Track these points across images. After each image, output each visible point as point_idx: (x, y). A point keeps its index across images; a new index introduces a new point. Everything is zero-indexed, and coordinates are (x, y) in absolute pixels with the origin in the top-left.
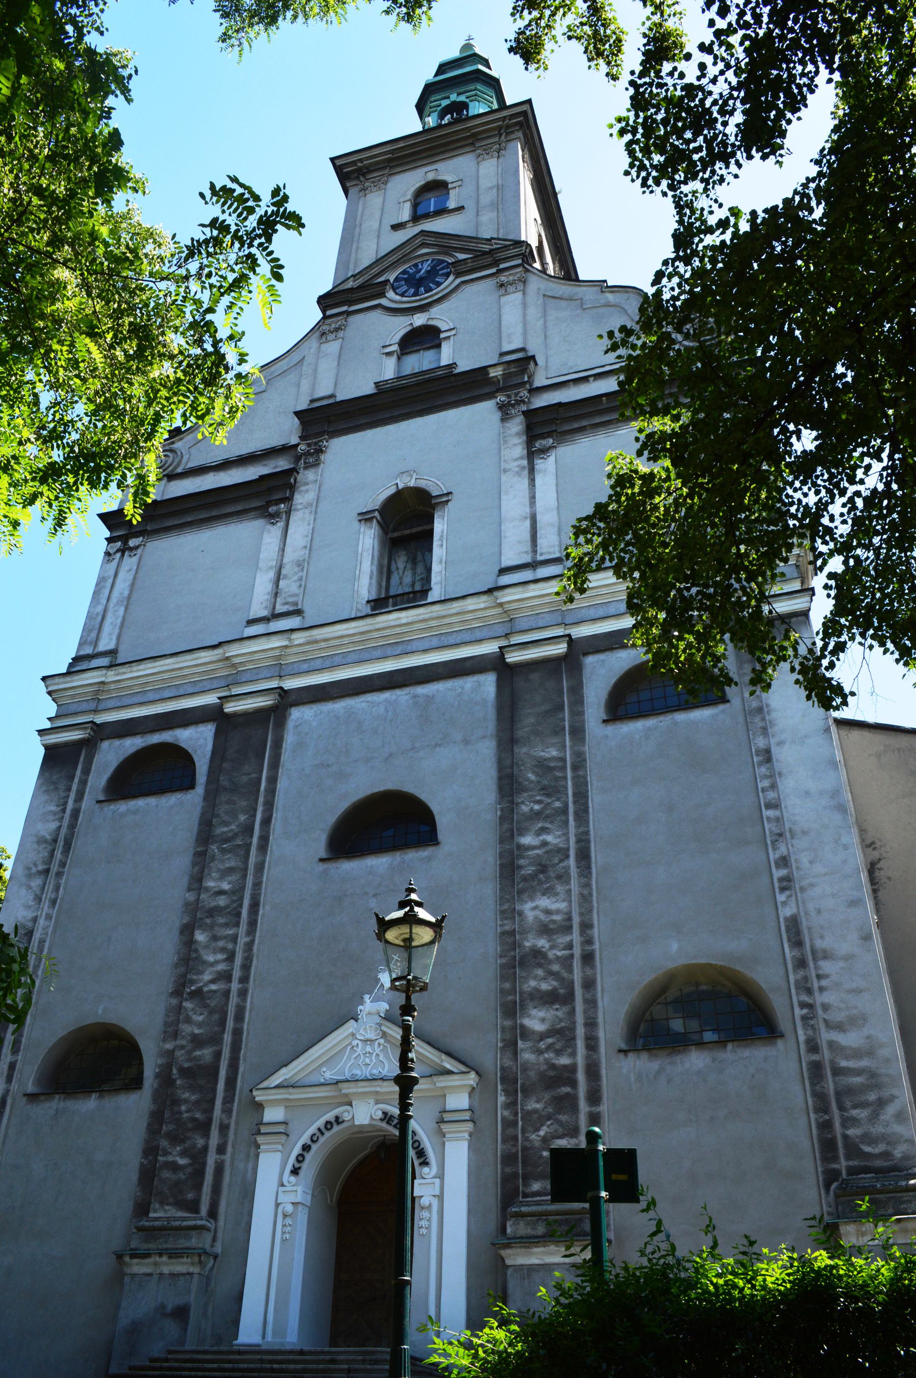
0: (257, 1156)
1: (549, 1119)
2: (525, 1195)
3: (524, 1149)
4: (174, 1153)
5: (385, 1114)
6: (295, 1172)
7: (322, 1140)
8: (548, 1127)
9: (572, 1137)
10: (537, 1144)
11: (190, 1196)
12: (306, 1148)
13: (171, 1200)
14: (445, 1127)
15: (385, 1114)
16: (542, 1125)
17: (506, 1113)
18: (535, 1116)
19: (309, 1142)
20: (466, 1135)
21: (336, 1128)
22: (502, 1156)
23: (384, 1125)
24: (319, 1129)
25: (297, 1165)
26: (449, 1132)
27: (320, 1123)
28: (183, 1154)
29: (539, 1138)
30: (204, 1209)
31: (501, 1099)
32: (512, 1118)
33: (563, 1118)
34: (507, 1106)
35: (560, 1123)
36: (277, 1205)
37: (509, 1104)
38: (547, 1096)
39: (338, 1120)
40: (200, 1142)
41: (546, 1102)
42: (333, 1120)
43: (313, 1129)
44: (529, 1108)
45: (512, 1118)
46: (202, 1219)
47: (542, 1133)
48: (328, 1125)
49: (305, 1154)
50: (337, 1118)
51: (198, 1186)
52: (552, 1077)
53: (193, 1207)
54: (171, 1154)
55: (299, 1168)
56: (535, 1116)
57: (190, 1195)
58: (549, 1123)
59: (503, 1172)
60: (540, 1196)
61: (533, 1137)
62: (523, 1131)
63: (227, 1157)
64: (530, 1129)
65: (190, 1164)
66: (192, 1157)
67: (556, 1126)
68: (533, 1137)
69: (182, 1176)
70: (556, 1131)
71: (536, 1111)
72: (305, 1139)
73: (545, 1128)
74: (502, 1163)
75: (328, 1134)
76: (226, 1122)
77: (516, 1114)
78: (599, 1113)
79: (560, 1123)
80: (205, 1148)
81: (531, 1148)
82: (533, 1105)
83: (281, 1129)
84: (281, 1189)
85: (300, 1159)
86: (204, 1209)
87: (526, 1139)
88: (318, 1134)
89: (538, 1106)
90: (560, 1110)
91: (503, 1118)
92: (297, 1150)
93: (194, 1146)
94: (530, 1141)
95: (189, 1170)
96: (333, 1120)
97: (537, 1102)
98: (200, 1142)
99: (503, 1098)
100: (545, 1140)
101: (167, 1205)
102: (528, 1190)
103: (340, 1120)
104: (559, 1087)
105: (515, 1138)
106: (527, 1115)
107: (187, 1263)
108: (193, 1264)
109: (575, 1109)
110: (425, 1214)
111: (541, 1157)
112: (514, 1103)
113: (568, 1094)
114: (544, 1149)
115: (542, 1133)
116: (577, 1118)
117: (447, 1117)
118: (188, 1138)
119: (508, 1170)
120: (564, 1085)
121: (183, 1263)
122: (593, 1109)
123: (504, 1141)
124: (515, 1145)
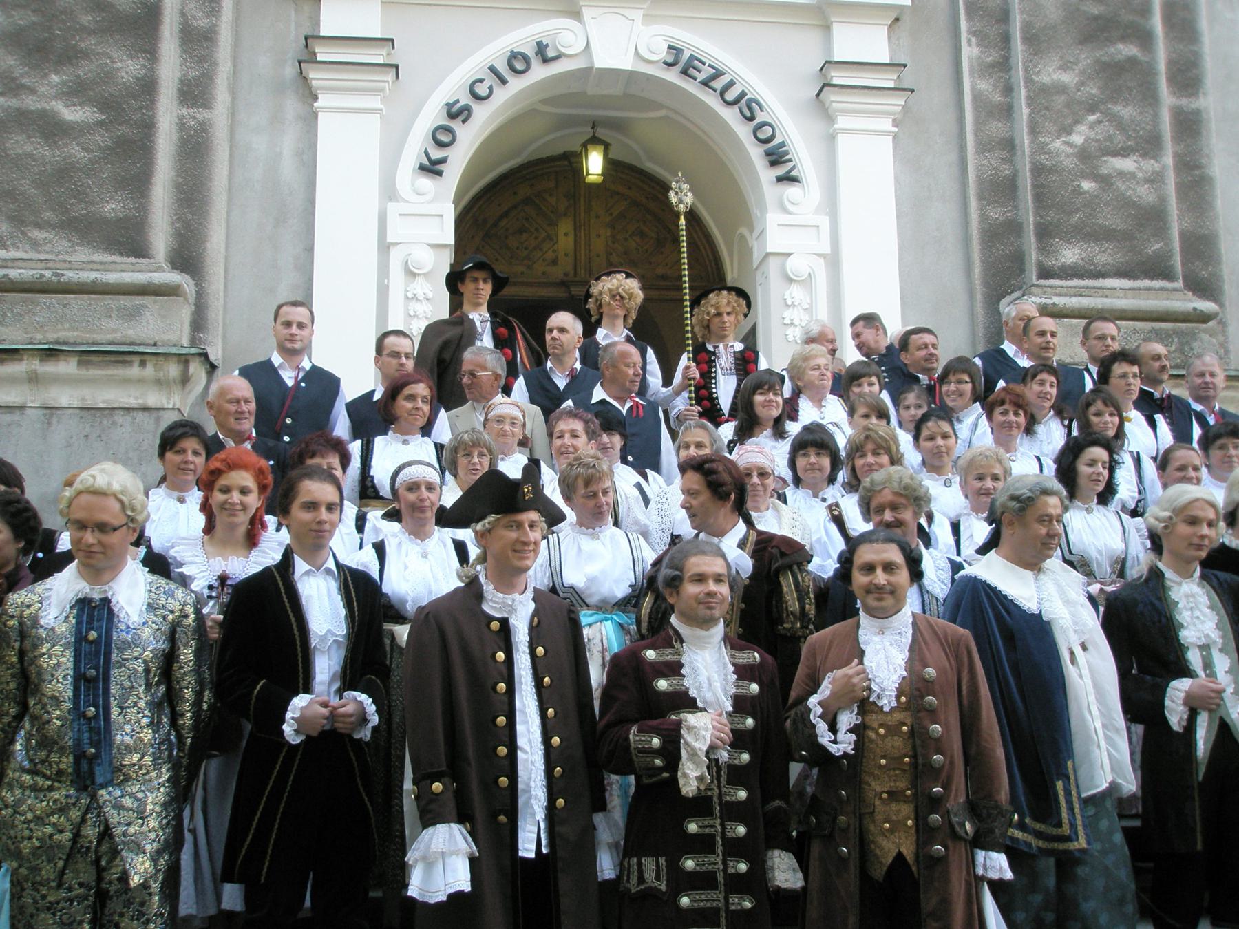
0: (311, 119)
1: (1092, 110)
2: (1045, 273)
3: (1038, 170)
4: (42, 89)
5: (675, 50)
6: (432, 168)
7: (502, 96)
8: (1091, 127)
9: (1145, 155)
10: (1069, 163)
11: (112, 208)
12: (458, 113)
13: (48, 215)
14: (831, 97)
15: (675, 50)
16: (1077, 122)
17: (983, 86)
18: (1060, 100)
19: (465, 99)
20: (887, 124)
21: (539, 72)
22: (980, 182)
23: (672, 76)
24: (492, 69)
25: (436, 154)
26: (845, 111)
27: (495, 51)
28: (76, 92)
29: (1070, 150)
30: (160, 239)
31: (970, 52)
32: (997, 98)
33: (1126, 112)
34: (985, 70)
35: (1115, 119)
36: (385, 248)
37: (992, 66)
38: (1086, 57)
39: (542, 53)
40: (129, 68)
41: (1083, 72)
42: (530, 51)
43: (473, 65)
44: (1045, 79)
45: (997, 98)
46: (159, 269)
47: (1077, 139)
48: (517, 63)
49: (455, 125)
50: (541, 49)
51: (139, 183)
52: (1096, 18)
53: (137, 248)
54: (32, 91)
55: (443, 161)
56: (1060, 100)
57: (109, 207)
58: (1092, 118)
59: (983, 217)
60: (1081, 277)
61: (1057, 144)
62: (1034, 130)
63: (219, 114)
64: (1049, 126)
65: (101, 124)
66: (105, 104)
67: (1107, 129)
68: (1057, 144)
69: (75, 152)
70: (1110, 138)
71: (1061, 89)
72: (452, 88)
73: (1082, 128)
74: (981, 197)
75: (517, 84)
76: (203, 23)
77: (1008, 90)
78: (1197, 112)
79: (1115, 119)
80: (148, 87)
81: (1052, 170)
82: (1051, 73)
83: (378, 56)
84: (392, 207)
85: (444, 138)
86: (160, 239)
87: (1041, 148)
88: (490, 80)
89: (1067, 78)
90: (1114, 93)
91: (977, 97)
92: (431, 115)
93: (108, 76)
94: (1050, 153)
95: (100, 139)
96: (530, 51)
97: (1064, 67)
98: (129, 68)
99: (976, 51)
100: (1084, 154)
101: (38, 226)
102: (1050, 262)
103: (550, 53)
104: (1113, 43)
105: (1009, 145)
106: (1041, 95)
107: (141, 381)
108: (159, 383)
109: (1149, 96)
110: (796, 293)
111: (1078, 191)
112: (1004, 65)
113: (1132, 61)
114: (1084, 176)
115: (1077, 139)
116: (1156, 115)
117: (838, 78)
118: (85, 55)
119: (996, 213)
120: (1124, 38)
121: (126, 382)
122: (1183, 102)
123: (984, 147)
124: (1009, 160)
